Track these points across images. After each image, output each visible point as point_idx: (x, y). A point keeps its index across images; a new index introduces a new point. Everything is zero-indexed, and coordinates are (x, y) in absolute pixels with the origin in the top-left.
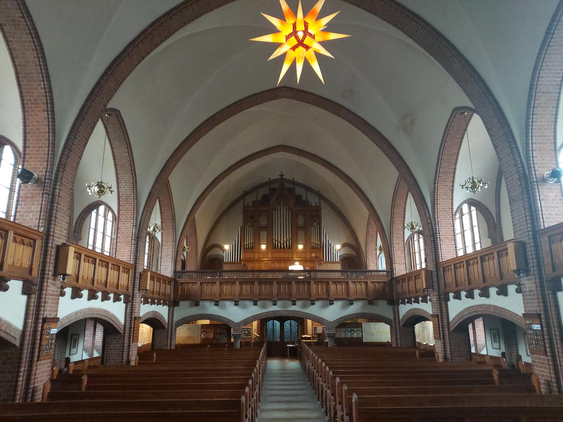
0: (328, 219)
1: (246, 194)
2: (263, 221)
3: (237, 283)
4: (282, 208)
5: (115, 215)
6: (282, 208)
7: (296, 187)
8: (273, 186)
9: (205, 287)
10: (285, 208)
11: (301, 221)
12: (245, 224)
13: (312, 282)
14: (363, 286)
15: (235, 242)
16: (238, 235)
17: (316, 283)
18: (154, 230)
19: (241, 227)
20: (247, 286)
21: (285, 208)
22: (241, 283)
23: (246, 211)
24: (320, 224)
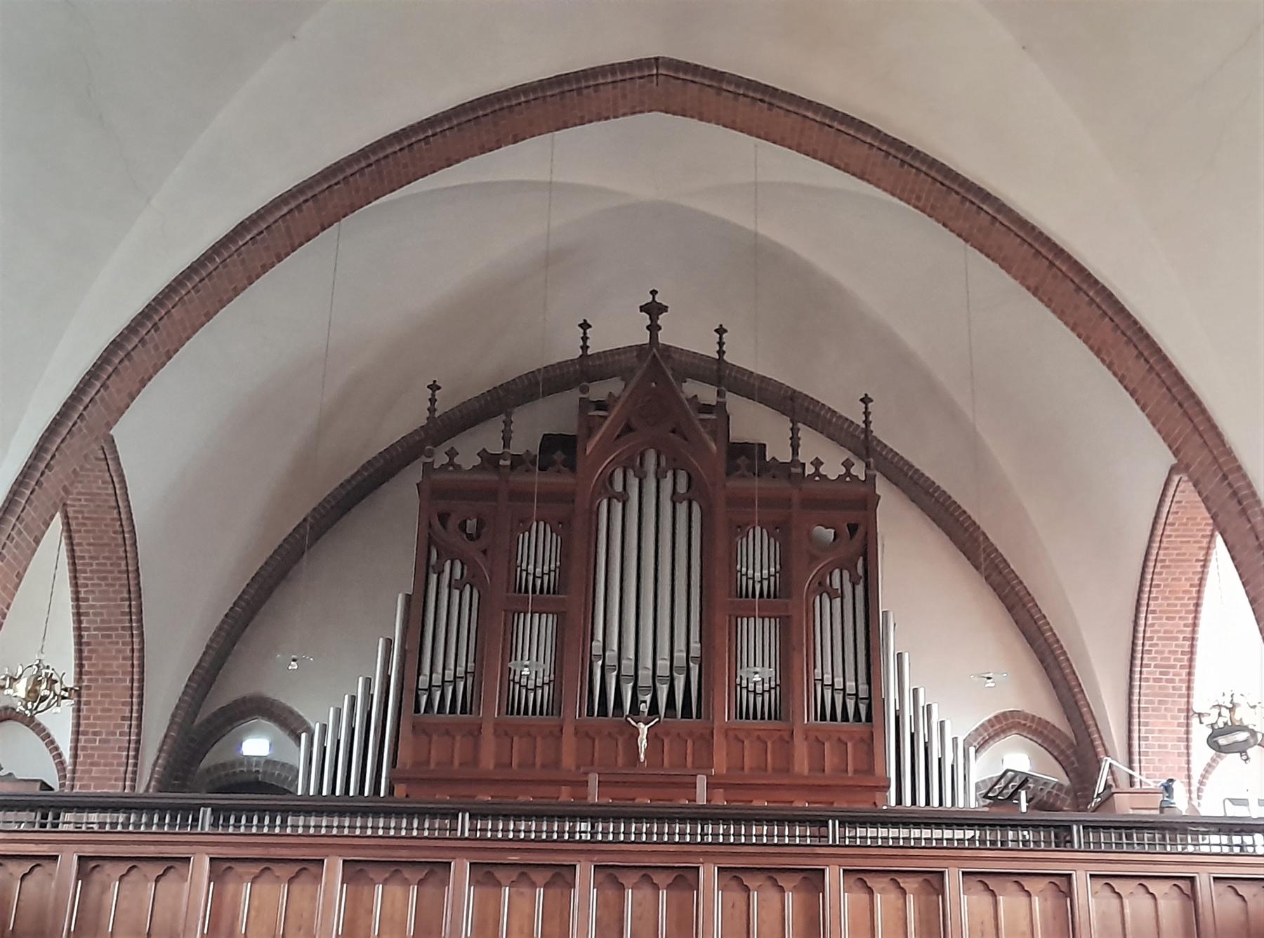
0: (915, 577)
1: (444, 427)
2: (537, 554)
3: (334, 868)
4: (651, 484)
5: (62, 763)
6: (651, 484)
7: (734, 403)
8: (599, 391)
9: (113, 890)
10: (667, 484)
11: (757, 560)
12: (425, 570)
13: (833, 875)
14: (1169, 902)
15: (368, 683)
16: (389, 643)
17: (858, 877)
18: (33, 695)
19: (408, 599)
20: (396, 890)
21: (667, 484)
22: (355, 871)
23: (432, 492)
24: (869, 583)
